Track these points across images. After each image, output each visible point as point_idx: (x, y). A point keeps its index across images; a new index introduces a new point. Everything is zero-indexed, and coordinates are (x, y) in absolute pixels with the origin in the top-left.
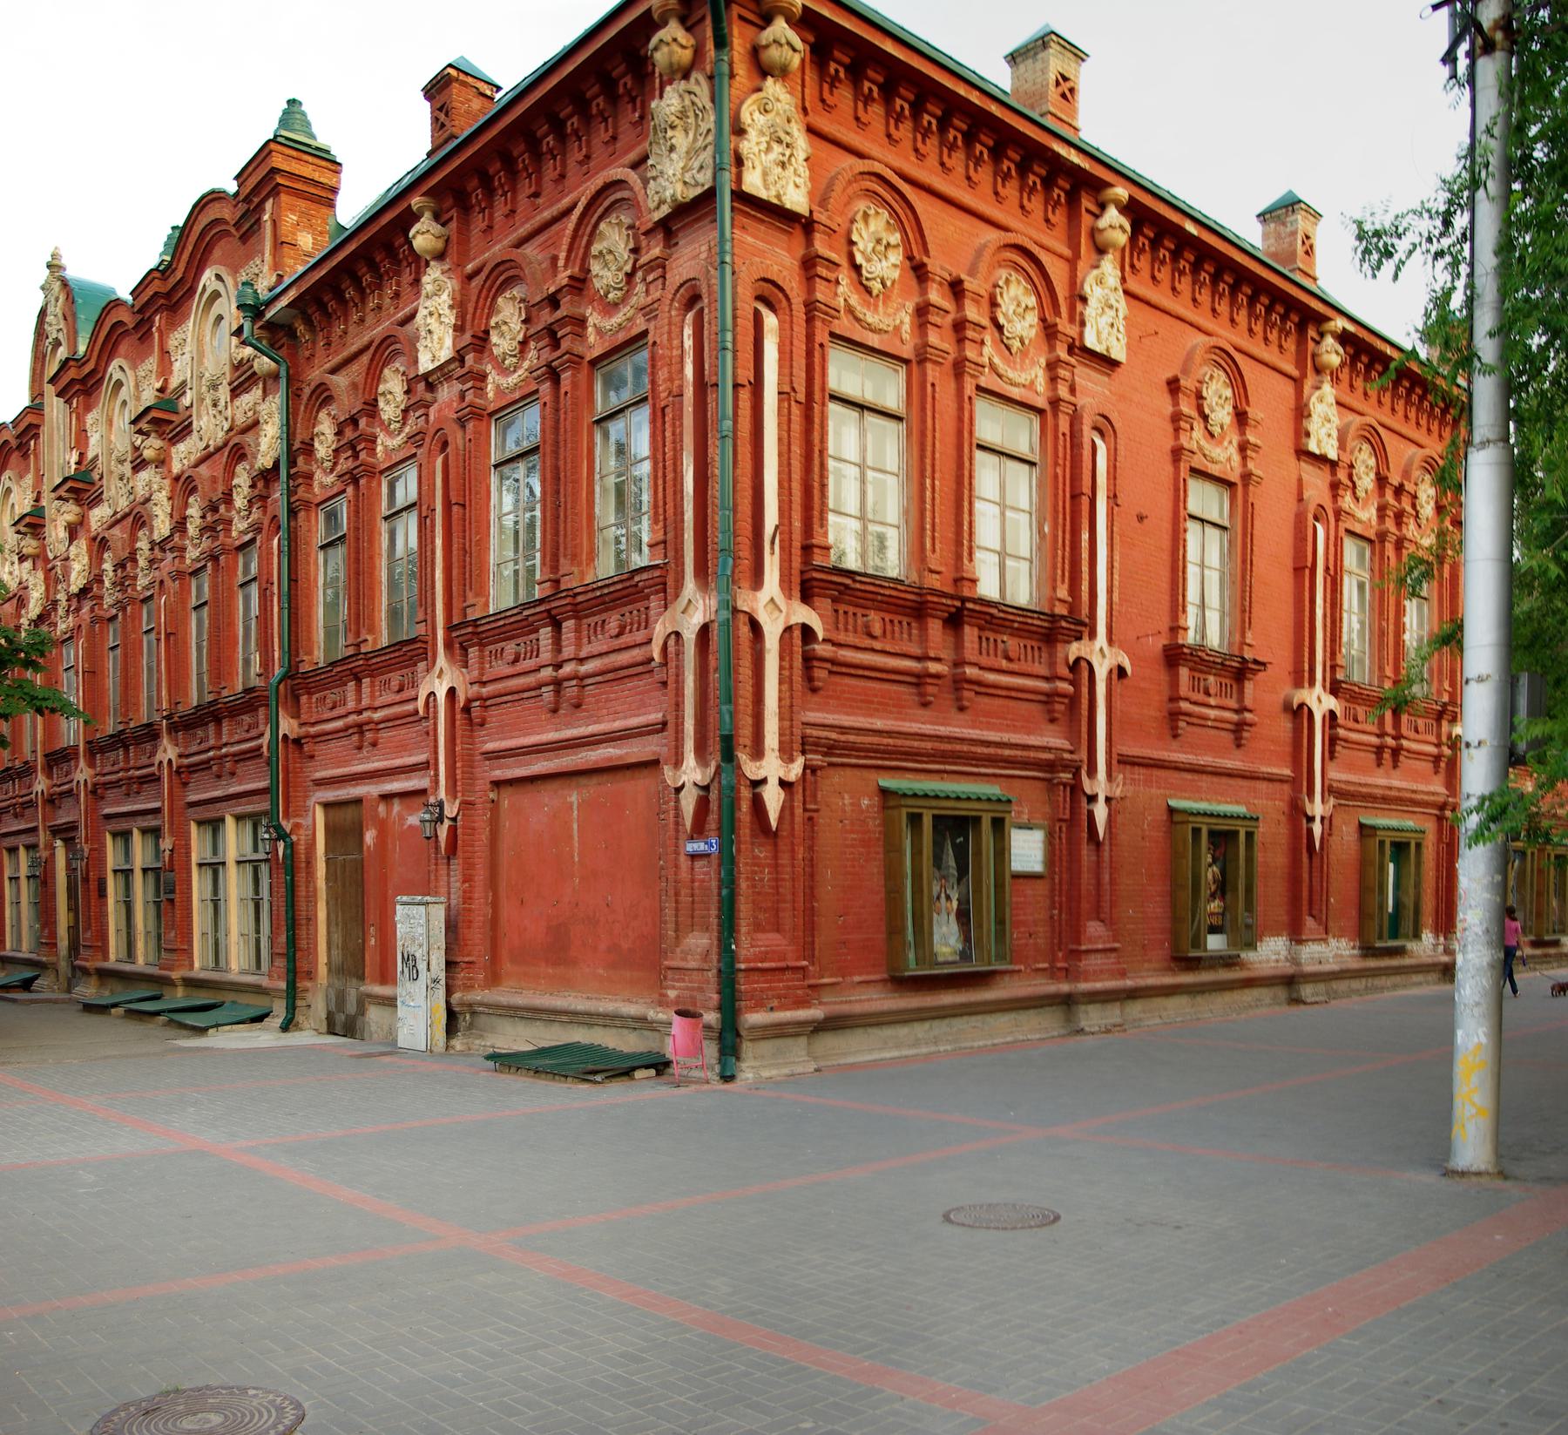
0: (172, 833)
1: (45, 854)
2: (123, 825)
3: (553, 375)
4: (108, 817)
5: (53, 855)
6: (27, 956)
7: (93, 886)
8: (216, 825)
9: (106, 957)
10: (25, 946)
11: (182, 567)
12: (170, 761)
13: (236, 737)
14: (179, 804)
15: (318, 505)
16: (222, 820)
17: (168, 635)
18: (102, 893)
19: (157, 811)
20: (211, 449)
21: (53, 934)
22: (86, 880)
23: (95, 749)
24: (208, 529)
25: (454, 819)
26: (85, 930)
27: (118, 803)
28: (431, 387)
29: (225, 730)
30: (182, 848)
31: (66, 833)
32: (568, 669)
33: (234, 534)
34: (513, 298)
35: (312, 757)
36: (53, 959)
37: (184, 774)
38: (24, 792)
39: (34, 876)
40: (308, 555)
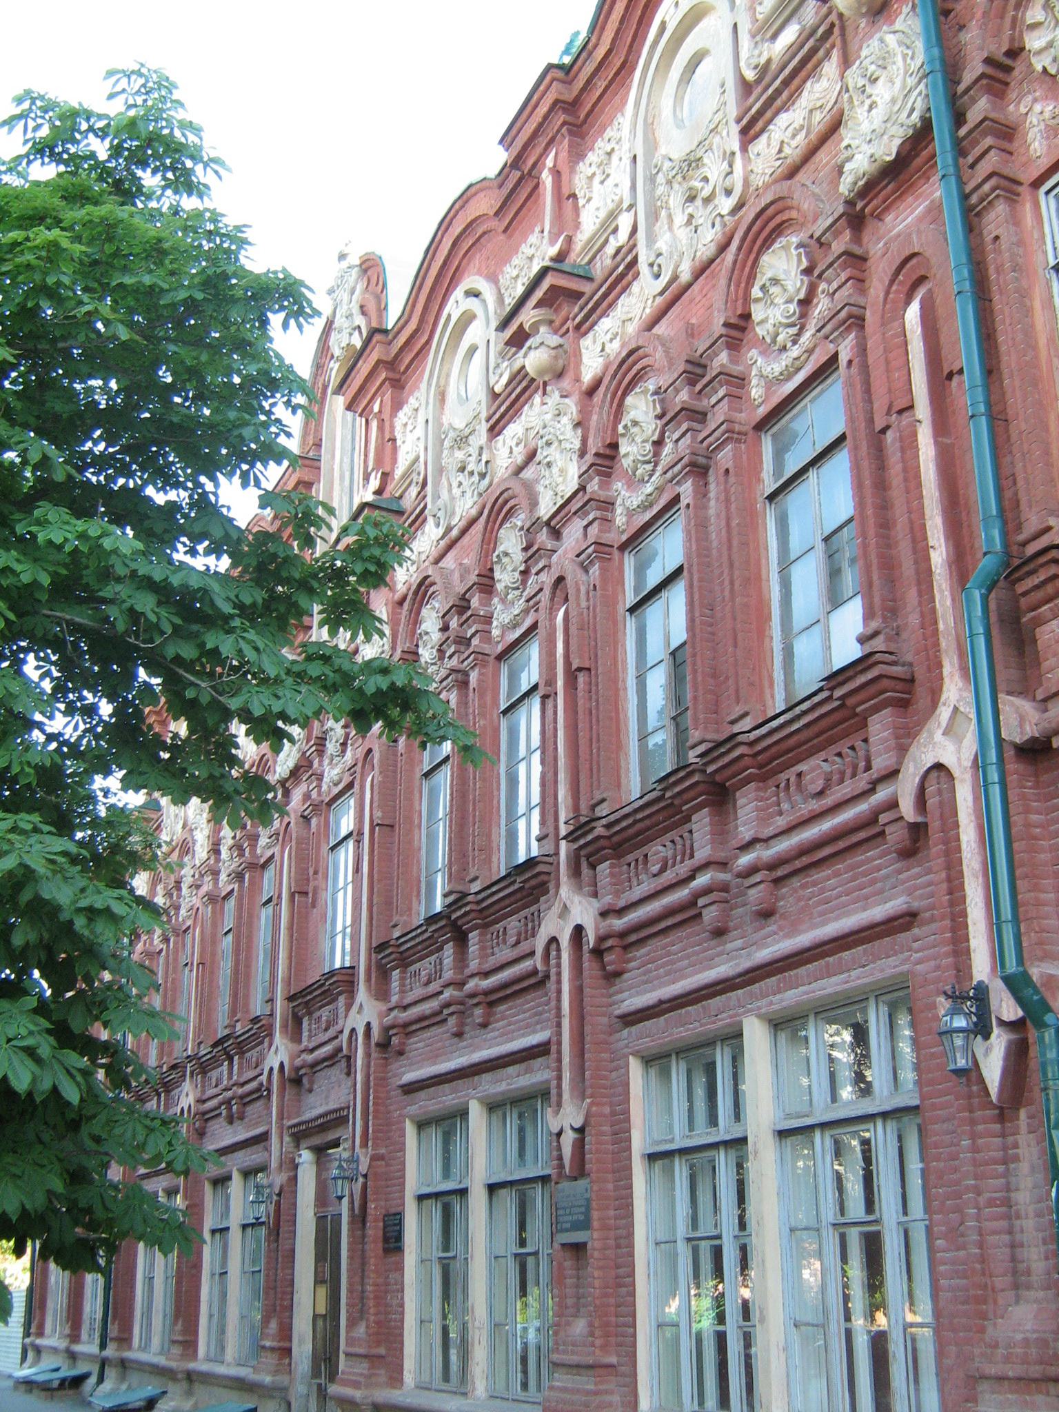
0: (580, 1092)
1: (279, 1179)
2: (446, 1098)
3: (699, 469)
4: (411, 1089)
5: (294, 1179)
6: (233, 1371)
7: (374, 1230)
8: (450, 1122)
9: (396, 1378)
10: (230, 1353)
11: (608, 538)
12: (579, 930)
13: (781, 822)
14: (598, 1022)
15: (1037, 184)
16: (464, 1114)
17: (572, 676)
18: (393, 1241)
19: (540, 1050)
20: (455, 533)
21: (286, 1332)
22: (360, 1219)
23: (602, 842)
24: (238, 847)
25: (365, 1176)
26: (352, 1324)
27: (435, 1057)
28: (556, 534)
29: (473, 949)
30: (386, 1171)
31: (320, 1134)
32: (471, 985)
33: (496, 632)
34: (645, 392)
35: (401, 1053)
36: (283, 1379)
37: (606, 955)
38: (251, 1074)
39: (257, 1224)
40: (1024, 294)
